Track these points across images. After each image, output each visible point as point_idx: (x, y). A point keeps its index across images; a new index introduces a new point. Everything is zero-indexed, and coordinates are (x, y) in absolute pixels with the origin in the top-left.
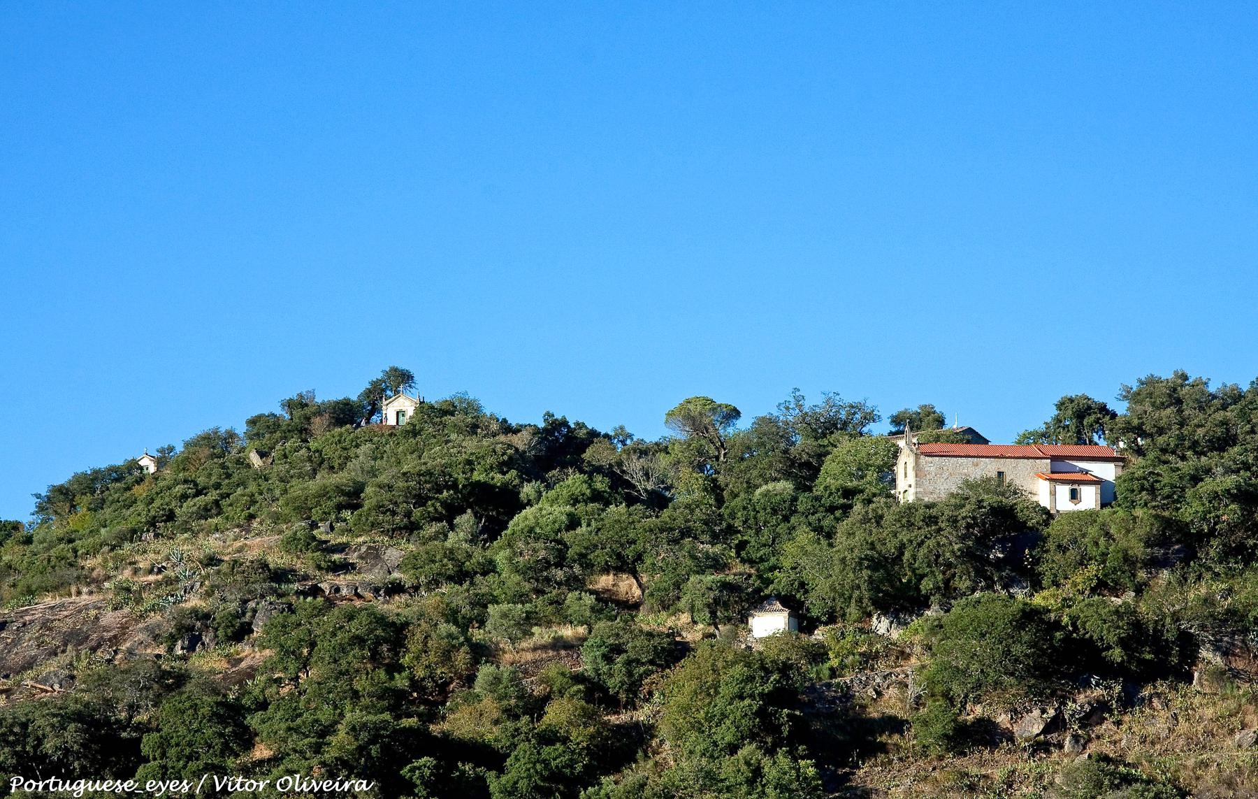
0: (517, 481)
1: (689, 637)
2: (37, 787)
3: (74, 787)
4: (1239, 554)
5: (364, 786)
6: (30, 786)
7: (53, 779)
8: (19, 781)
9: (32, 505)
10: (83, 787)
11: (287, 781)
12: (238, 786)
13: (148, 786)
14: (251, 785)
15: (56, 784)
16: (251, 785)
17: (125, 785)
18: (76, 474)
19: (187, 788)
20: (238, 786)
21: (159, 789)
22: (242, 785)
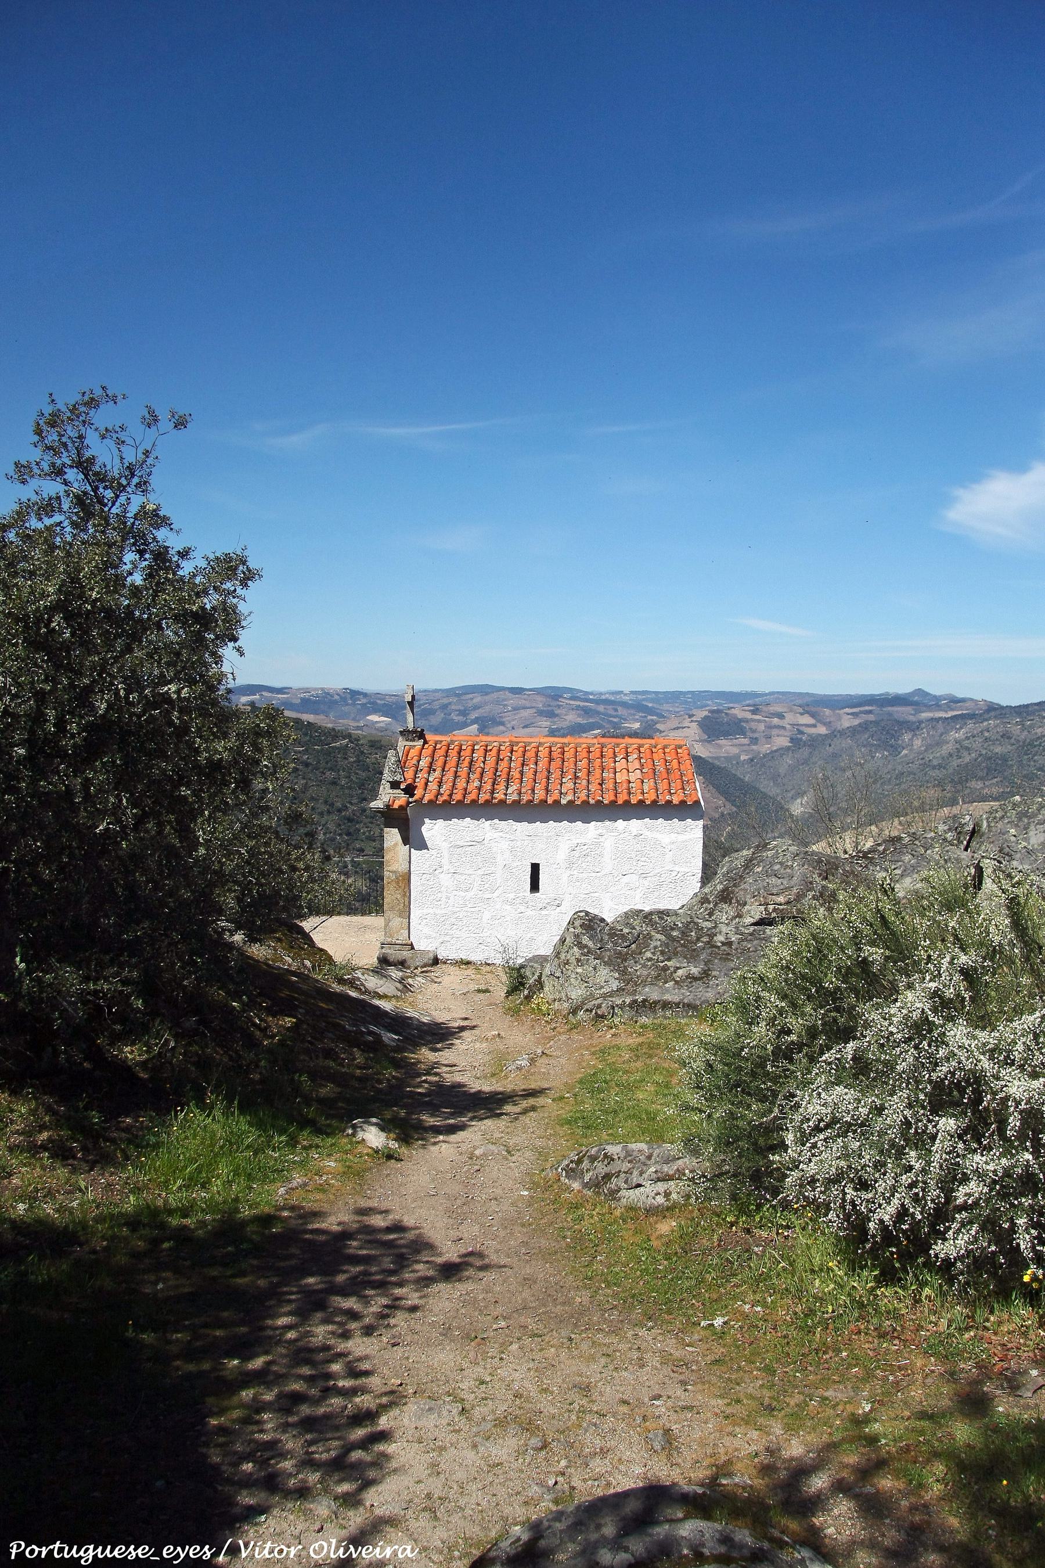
0: (648, 1539)
1: (789, 1151)
2: (40, 1552)
3: (82, 1553)
4: (995, 1277)
5: (408, 1551)
6: (32, 1552)
7: (58, 1544)
8: (19, 1546)
9: (242, 608)
10: (88, 1554)
11: (322, 1548)
12: (266, 1551)
13: (165, 1552)
14: (281, 1551)
15: (61, 1550)
16: (281, 1551)
17: (139, 1551)
18: (887, 694)
19: (209, 1554)
20: (266, 1551)
21: (178, 1556)
22: (271, 1552)
